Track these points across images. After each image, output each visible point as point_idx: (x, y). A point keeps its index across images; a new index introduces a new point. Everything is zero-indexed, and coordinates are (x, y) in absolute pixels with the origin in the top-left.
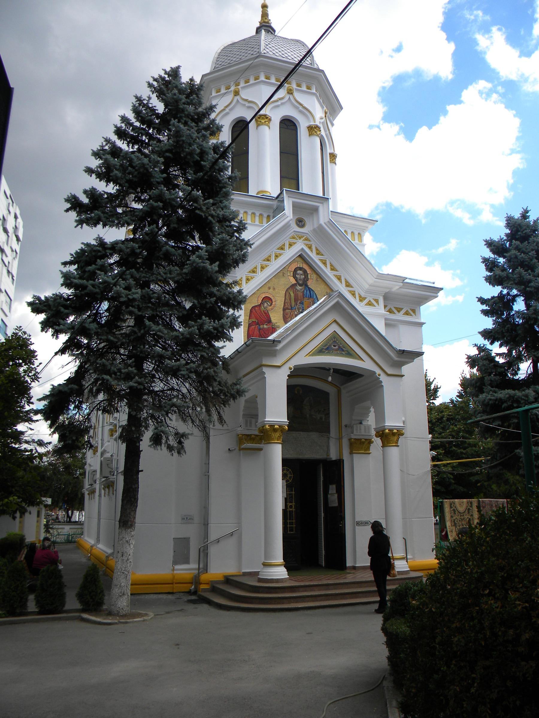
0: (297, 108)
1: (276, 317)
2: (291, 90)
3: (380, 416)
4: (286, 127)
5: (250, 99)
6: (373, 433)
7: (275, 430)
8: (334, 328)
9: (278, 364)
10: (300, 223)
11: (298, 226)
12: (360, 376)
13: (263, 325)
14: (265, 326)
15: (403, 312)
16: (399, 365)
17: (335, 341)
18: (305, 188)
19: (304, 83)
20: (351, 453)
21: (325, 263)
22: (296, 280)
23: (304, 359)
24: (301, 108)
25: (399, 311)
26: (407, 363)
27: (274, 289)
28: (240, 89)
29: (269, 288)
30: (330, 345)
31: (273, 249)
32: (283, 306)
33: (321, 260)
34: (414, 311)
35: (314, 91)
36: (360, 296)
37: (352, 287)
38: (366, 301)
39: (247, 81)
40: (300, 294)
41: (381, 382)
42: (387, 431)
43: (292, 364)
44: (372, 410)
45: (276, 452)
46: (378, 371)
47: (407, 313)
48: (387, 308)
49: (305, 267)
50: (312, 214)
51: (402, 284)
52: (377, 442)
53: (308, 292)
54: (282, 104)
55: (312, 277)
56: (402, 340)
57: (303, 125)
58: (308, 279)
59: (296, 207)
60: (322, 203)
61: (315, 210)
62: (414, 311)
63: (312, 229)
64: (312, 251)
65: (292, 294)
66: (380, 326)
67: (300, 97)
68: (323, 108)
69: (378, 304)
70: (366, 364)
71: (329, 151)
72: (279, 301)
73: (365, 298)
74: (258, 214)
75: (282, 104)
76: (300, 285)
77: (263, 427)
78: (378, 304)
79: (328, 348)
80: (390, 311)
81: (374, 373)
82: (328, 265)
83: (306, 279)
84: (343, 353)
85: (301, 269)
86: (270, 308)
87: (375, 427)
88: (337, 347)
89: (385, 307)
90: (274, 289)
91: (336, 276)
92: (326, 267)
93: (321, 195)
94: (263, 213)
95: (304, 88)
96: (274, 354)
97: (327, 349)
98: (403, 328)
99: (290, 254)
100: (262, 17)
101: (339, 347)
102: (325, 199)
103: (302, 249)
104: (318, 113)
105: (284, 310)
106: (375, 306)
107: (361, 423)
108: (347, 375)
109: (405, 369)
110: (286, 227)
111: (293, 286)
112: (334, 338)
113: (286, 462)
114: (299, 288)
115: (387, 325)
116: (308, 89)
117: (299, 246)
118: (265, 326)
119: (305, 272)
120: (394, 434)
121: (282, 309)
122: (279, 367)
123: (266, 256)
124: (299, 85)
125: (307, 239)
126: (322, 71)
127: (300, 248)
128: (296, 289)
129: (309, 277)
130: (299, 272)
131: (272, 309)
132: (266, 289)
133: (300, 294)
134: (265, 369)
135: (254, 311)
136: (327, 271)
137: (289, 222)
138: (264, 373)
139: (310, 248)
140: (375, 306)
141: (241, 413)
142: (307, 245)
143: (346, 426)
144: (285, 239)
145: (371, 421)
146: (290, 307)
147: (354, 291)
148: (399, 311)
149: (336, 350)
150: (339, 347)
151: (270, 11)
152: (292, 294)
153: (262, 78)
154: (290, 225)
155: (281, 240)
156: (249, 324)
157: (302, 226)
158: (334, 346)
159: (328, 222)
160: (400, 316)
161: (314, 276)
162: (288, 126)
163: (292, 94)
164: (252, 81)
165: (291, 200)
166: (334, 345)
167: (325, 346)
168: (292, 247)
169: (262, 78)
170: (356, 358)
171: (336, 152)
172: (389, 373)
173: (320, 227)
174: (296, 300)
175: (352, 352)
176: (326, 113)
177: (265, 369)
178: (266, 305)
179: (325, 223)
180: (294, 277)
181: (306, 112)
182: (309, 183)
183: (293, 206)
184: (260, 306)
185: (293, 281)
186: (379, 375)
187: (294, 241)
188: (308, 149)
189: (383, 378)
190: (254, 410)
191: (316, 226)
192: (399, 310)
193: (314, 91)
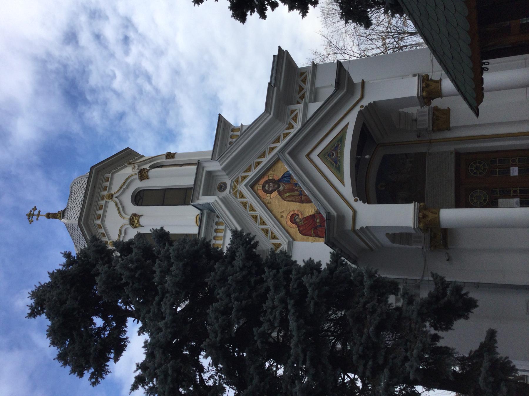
0: (124, 190)
1: (308, 210)
2: (109, 196)
3: (406, 101)
4: (141, 200)
5: (118, 232)
6: (426, 109)
7: (424, 216)
8: (315, 156)
9: (351, 212)
10: (222, 187)
11: (225, 189)
12: (364, 124)
13: (316, 222)
14: (318, 221)
15: (302, 84)
16: (351, 85)
17: (328, 155)
18: (189, 182)
19: (103, 184)
20: (448, 129)
21: (259, 163)
22: (275, 191)
23: (347, 190)
24: (124, 187)
25: (303, 89)
26: (349, 78)
27: (283, 212)
28: (111, 241)
29: (282, 216)
30: (332, 159)
31: (247, 214)
32: (298, 204)
33: (256, 166)
34: (302, 74)
35: (110, 175)
36: (288, 128)
37: (280, 136)
38: (293, 122)
39: (103, 235)
40: (288, 187)
41: (370, 104)
42: (424, 94)
43: (350, 198)
44: (400, 110)
45: (449, 216)
46: (357, 109)
47: (304, 81)
48: (299, 100)
49: (262, 181)
50: (213, 176)
51: (275, 88)
52: (436, 102)
53: (285, 179)
54: (121, 204)
55: (271, 175)
56: (326, 85)
57: (138, 185)
58: (273, 179)
59: (207, 192)
60: (203, 168)
61: (210, 174)
62: (302, 72)
63: (227, 177)
64: (247, 176)
65: (288, 194)
66: (313, 107)
67: (114, 189)
68: (126, 167)
69: (296, 110)
70: (352, 119)
71: (163, 160)
72: (294, 207)
73: (290, 123)
74: (216, 227)
75: (121, 204)
76: (279, 187)
77: (420, 229)
78: (296, 110)
79: (335, 162)
80: (303, 97)
81: (360, 112)
82: (260, 160)
83: (273, 181)
84: (339, 146)
85: (264, 187)
86: (300, 216)
87: (420, 107)
88: (334, 153)
89: (298, 103)
90: (283, 212)
91: (270, 152)
92: (261, 162)
93: (195, 167)
94: (215, 222)
95: (108, 184)
96: (341, 218)
97: (336, 163)
98: (318, 84)
99: (250, 198)
100: (57, 218)
101: (334, 150)
102: (199, 164)
103: (245, 185)
104: (129, 171)
105: (302, 202)
106: (297, 113)
107: (416, 120)
108: (364, 138)
109: (356, 79)
110: (225, 201)
111: (280, 193)
112: (325, 155)
113: (458, 205)
114: (281, 188)
115: (315, 100)
116: (108, 180)
117: (242, 188)
118: (318, 221)
119: (266, 182)
120: (428, 86)
121: (302, 205)
122: (355, 213)
123: (253, 220)
124: (105, 189)
125: (237, 182)
126: (92, 168)
127: (244, 187)
128: (283, 190)
129: (271, 178)
130: (267, 188)
131: (302, 214)
132: (283, 220)
133: (288, 187)
134: (358, 227)
135: (303, 232)
136: (265, 161)
137: (221, 199)
138: (362, 228)
139: (244, 178)
140: (297, 113)
141: (407, 246)
142: (242, 181)
143: (419, 137)
144: (237, 202)
145: (414, 110)
146: (300, 197)
147: (284, 134)
148: (303, 89)
149: (337, 153)
150: (334, 150)
151: (52, 211)
152: (288, 194)
153: (99, 222)
154: (224, 197)
155: (237, 205)
156: (316, 237)
157: (225, 185)
158: (333, 155)
159: (219, 161)
160: (307, 88)
161: (271, 173)
162: (141, 198)
163: (112, 195)
164: (102, 231)
165: (201, 197)
166: (332, 156)
167: (333, 165)
168: (244, 195)
169: (99, 222)
170: (346, 132)
171: (165, 153)
172: (358, 96)
173: (224, 169)
174: (293, 190)
175: (339, 136)
176: (130, 163)
177: (358, 227)
178: (298, 220)
179: (221, 165)
180: (271, 192)
181: (127, 183)
182: (185, 178)
183: (207, 195)
184: (299, 226)
185: (275, 193)
186: (362, 106)
187: (238, 194)
188: (159, 179)
189: (365, 102)
190: (399, 236)
191: (224, 173)
192: (301, 89)
193: (110, 175)
